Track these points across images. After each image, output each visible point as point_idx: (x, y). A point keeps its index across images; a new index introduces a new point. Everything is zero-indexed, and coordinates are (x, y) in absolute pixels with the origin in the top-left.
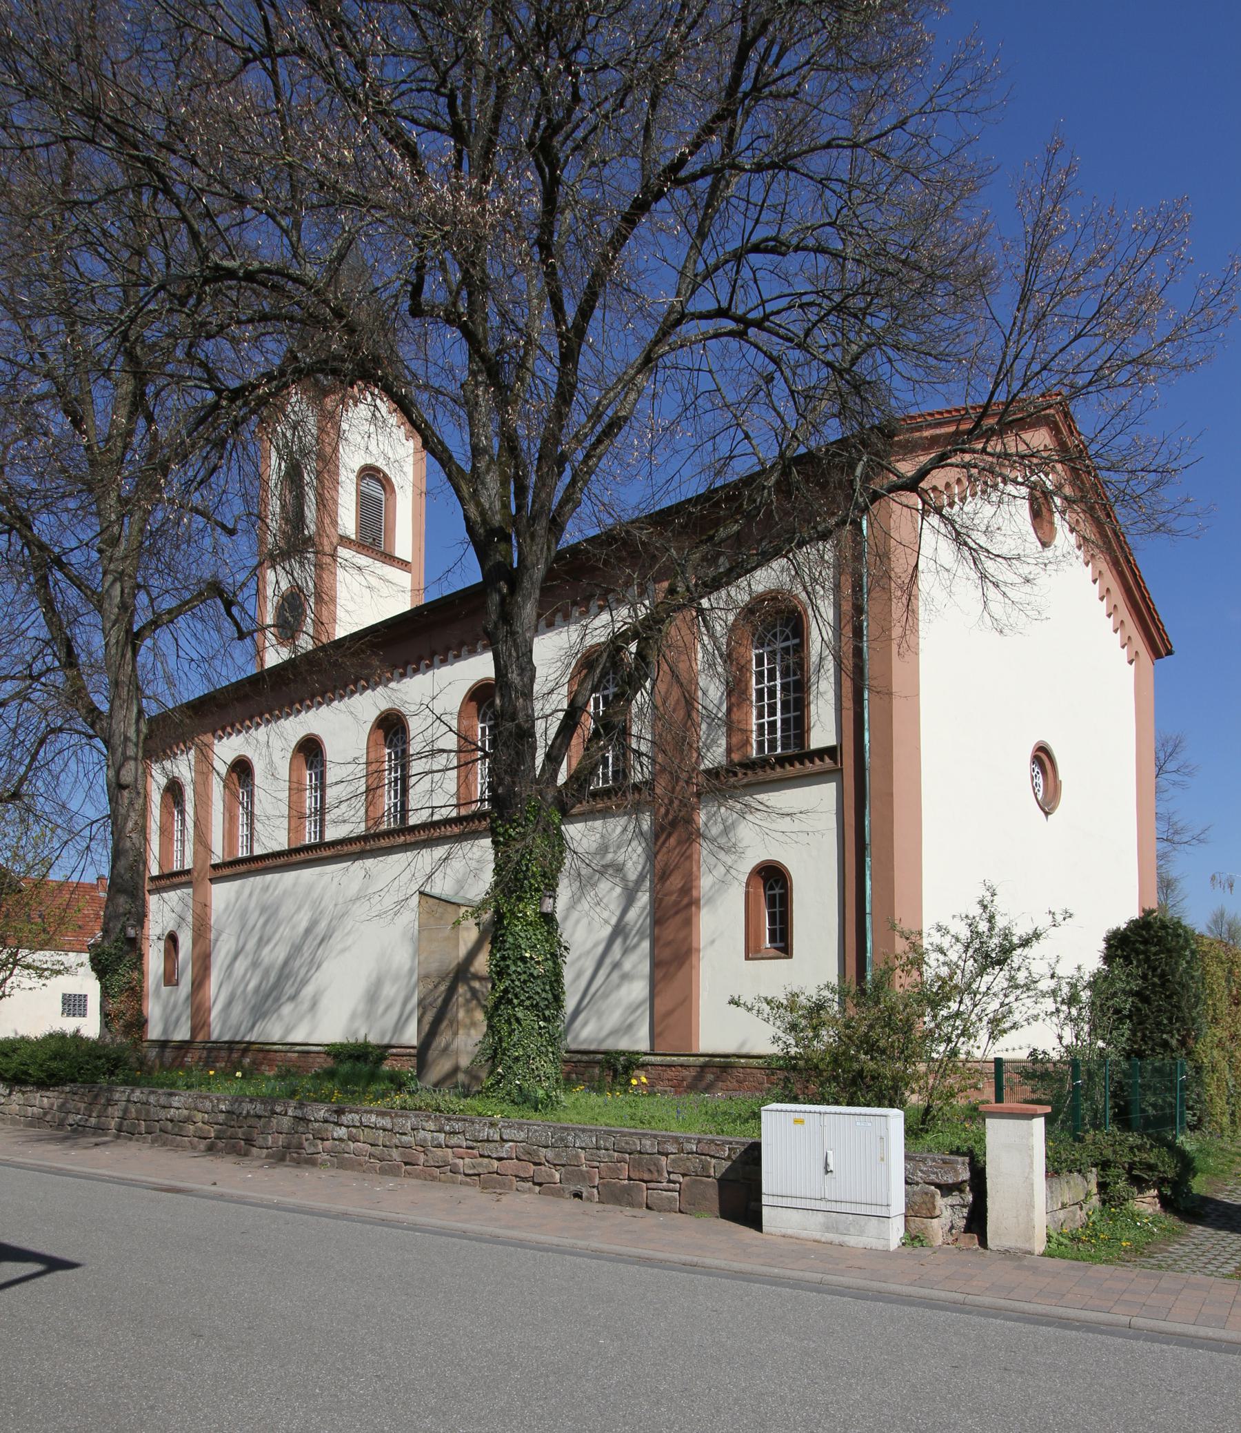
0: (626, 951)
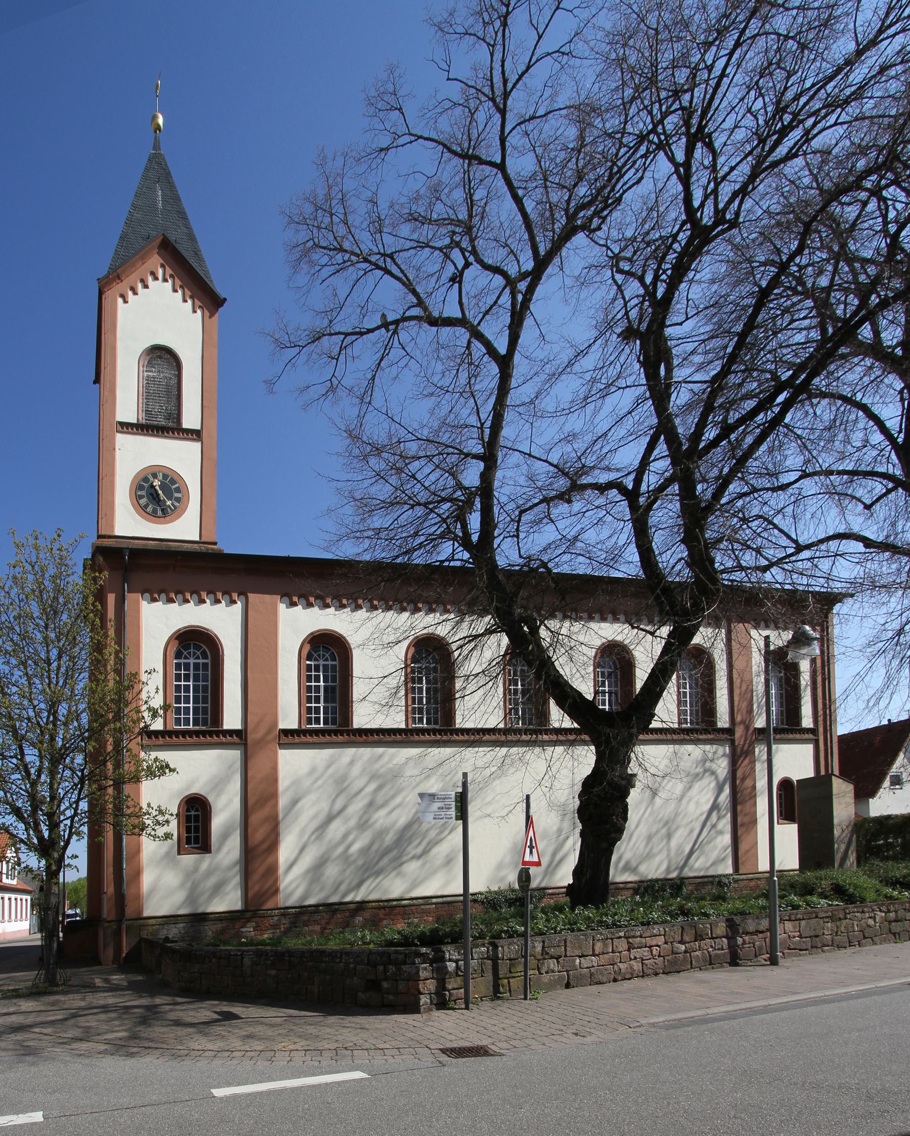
0: (719, 818)
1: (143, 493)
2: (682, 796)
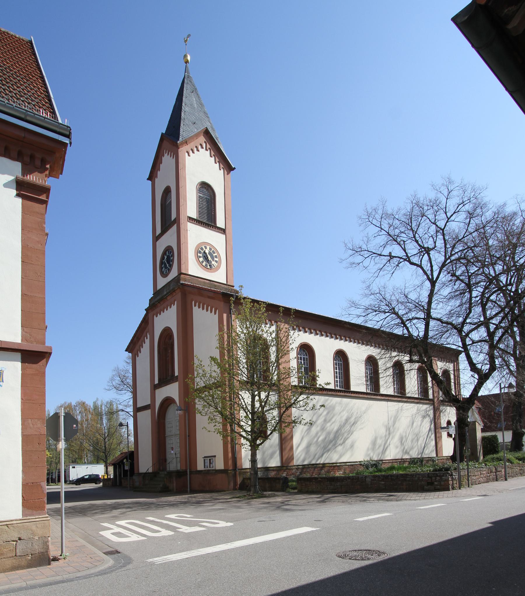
1: (201, 255)
2: (421, 425)
